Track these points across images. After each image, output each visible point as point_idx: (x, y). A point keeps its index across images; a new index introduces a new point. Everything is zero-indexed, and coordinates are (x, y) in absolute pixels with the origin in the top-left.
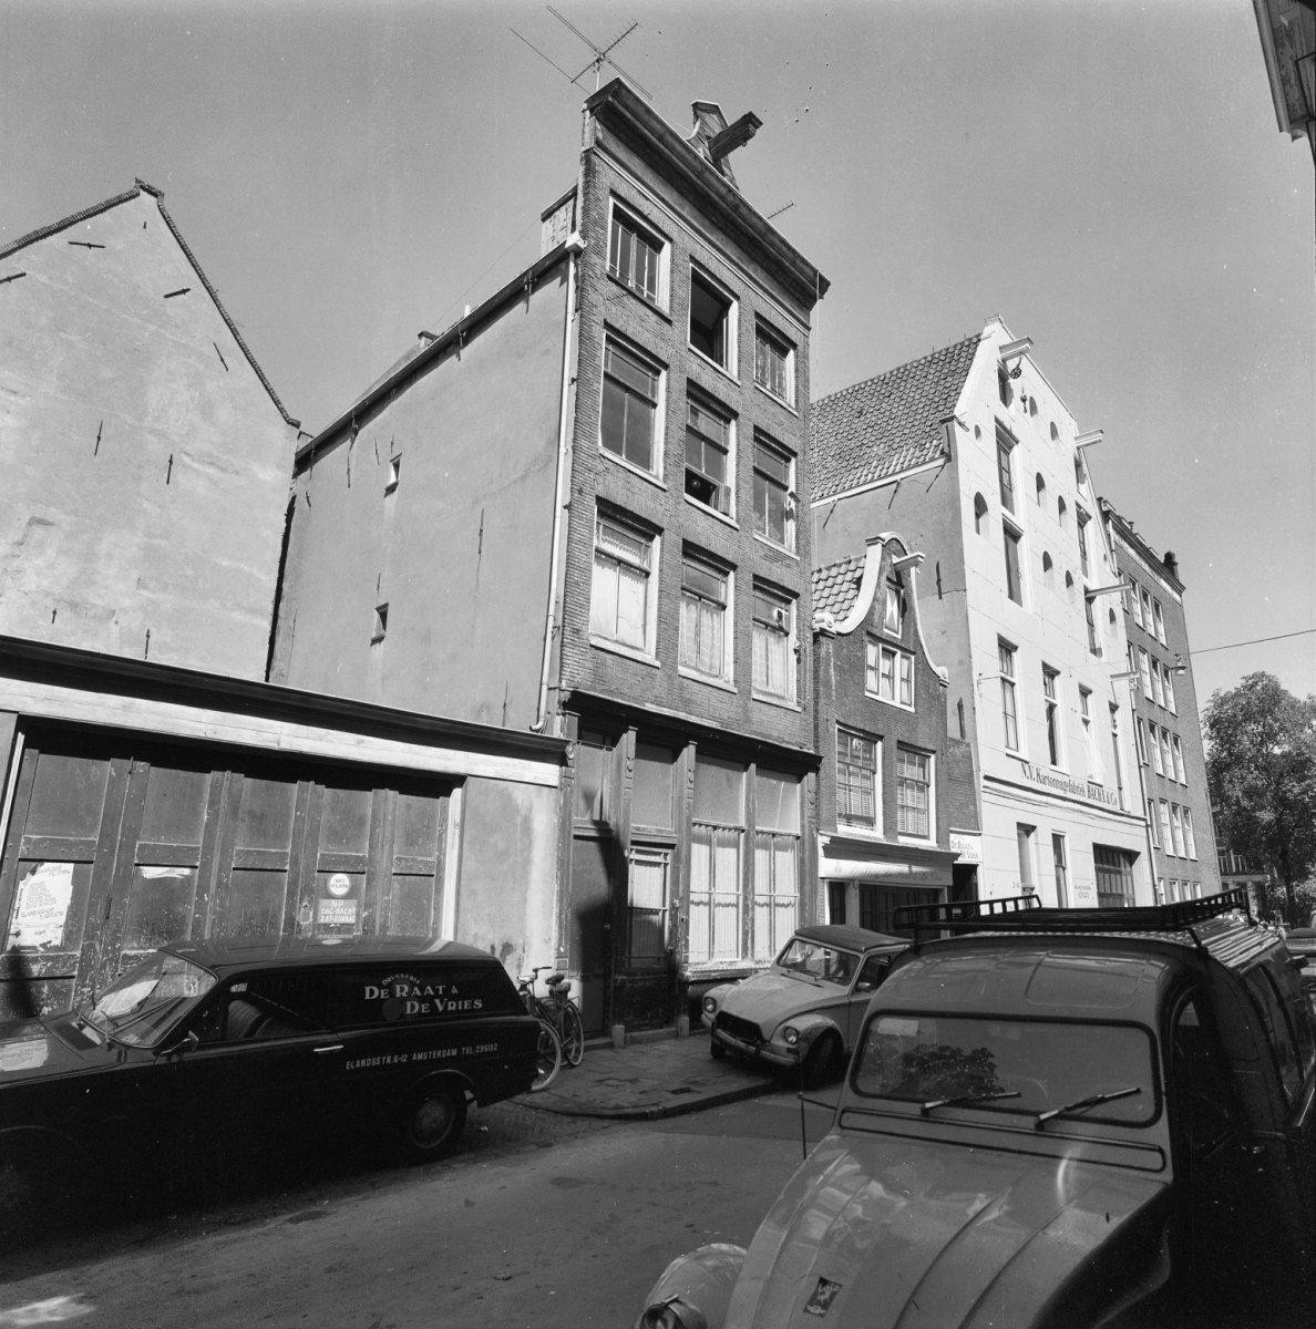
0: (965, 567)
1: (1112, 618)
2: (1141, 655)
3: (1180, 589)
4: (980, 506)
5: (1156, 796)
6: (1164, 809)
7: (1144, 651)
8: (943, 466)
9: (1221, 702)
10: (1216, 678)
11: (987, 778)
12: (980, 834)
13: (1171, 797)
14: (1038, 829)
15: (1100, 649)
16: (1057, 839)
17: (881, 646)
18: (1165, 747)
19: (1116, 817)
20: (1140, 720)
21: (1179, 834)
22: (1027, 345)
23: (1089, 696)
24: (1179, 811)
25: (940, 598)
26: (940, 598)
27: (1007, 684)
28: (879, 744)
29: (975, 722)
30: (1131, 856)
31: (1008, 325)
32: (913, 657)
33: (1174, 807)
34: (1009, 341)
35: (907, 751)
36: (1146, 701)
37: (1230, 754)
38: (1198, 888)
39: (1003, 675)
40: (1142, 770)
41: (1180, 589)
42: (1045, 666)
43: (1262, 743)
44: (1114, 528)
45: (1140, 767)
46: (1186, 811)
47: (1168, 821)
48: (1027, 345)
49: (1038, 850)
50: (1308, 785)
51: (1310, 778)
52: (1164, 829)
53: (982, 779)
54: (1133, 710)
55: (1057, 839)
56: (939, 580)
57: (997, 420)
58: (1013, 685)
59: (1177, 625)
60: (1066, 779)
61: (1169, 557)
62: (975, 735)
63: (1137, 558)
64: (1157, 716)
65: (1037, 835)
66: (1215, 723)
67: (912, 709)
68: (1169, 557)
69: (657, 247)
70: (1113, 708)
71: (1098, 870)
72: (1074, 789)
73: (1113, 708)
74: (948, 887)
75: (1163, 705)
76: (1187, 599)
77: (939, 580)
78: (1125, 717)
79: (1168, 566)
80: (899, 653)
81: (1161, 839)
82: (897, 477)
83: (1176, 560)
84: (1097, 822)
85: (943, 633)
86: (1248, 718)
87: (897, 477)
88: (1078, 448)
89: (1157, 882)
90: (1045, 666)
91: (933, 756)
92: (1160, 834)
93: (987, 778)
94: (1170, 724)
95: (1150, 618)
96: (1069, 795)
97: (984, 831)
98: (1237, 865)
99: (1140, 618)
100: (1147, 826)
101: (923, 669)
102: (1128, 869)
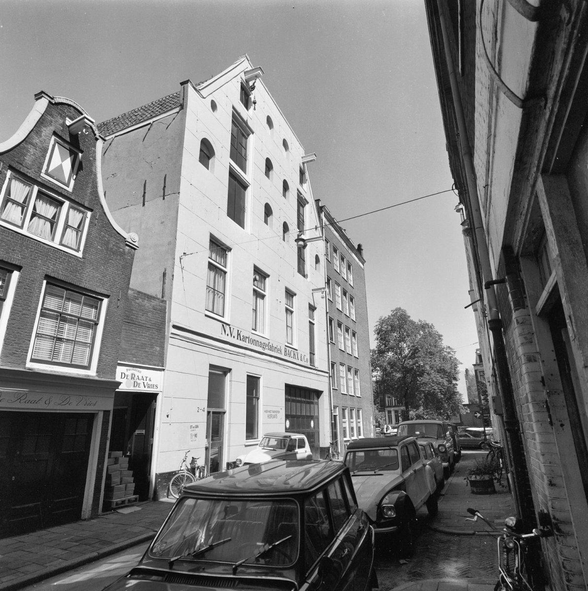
0: (181, 177)
1: (317, 260)
2: (336, 287)
3: (363, 262)
4: (207, 152)
5: (338, 360)
6: (343, 369)
7: (339, 285)
8: (178, 113)
9: (382, 322)
10: (378, 311)
11: (175, 327)
12: (164, 370)
13: (347, 363)
14: (233, 371)
15: (307, 275)
16: (253, 382)
17: (36, 188)
18: (347, 336)
19: (309, 370)
20: (331, 321)
21: (351, 383)
22: (259, 71)
23: (294, 297)
24: (353, 371)
25: (164, 199)
26: (164, 199)
27: (289, 312)
28: (16, 275)
29: (172, 285)
30: (318, 393)
31: (251, 61)
32: (89, 214)
33: (349, 369)
34: (250, 68)
35: (67, 289)
36: (352, 321)
37: (386, 346)
38: (361, 412)
39: (287, 306)
40: (329, 345)
41: (363, 262)
42: (257, 270)
43: (400, 341)
44: (325, 216)
45: (328, 344)
46: (356, 372)
47: (345, 376)
48: (259, 71)
49: (231, 385)
50: (417, 361)
51: (418, 357)
52: (341, 379)
53: (171, 327)
54: (327, 313)
55: (253, 382)
56: (165, 187)
57: (233, 108)
58: (225, 273)
59: (360, 276)
60: (266, 342)
61: (359, 246)
62: (171, 295)
63: (339, 238)
64: (343, 319)
65: (231, 375)
66: (379, 332)
67: (80, 255)
68: (359, 246)
69: (328, 243)
70: (312, 308)
71: (287, 400)
72: (271, 348)
73: (312, 308)
74: (106, 413)
75: (348, 315)
76: (367, 267)
77: (165, 187)
78: (320, 318)
79: (359, 250)
80: (67, 203)
81: (339, 385)
82: (151, 121)
83: (363, 248)
84: (290, 371)
85: (162, 223)
86: (393, 329)
87: (151, 121)
88: (303, 163)
89: (333, 409)
90: (257, 270)
91: (106, 301)
92: (339, 382)
93: (175, 327)
94: (351, 325)
95: (345, 270)
96: (267, 351)
97: (168, 366)
98: (395, 403)
99: (338, 268)
100: (330, 377)
101: (101, 224)
102: (317, 401)
